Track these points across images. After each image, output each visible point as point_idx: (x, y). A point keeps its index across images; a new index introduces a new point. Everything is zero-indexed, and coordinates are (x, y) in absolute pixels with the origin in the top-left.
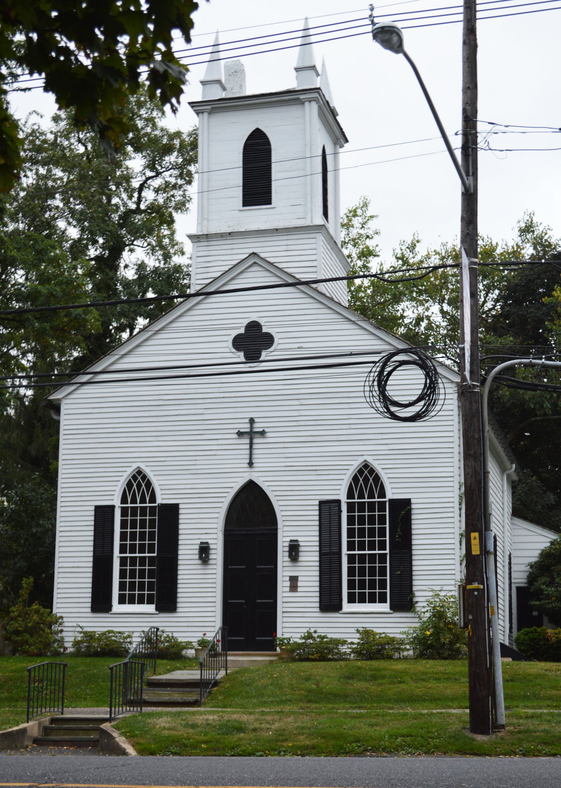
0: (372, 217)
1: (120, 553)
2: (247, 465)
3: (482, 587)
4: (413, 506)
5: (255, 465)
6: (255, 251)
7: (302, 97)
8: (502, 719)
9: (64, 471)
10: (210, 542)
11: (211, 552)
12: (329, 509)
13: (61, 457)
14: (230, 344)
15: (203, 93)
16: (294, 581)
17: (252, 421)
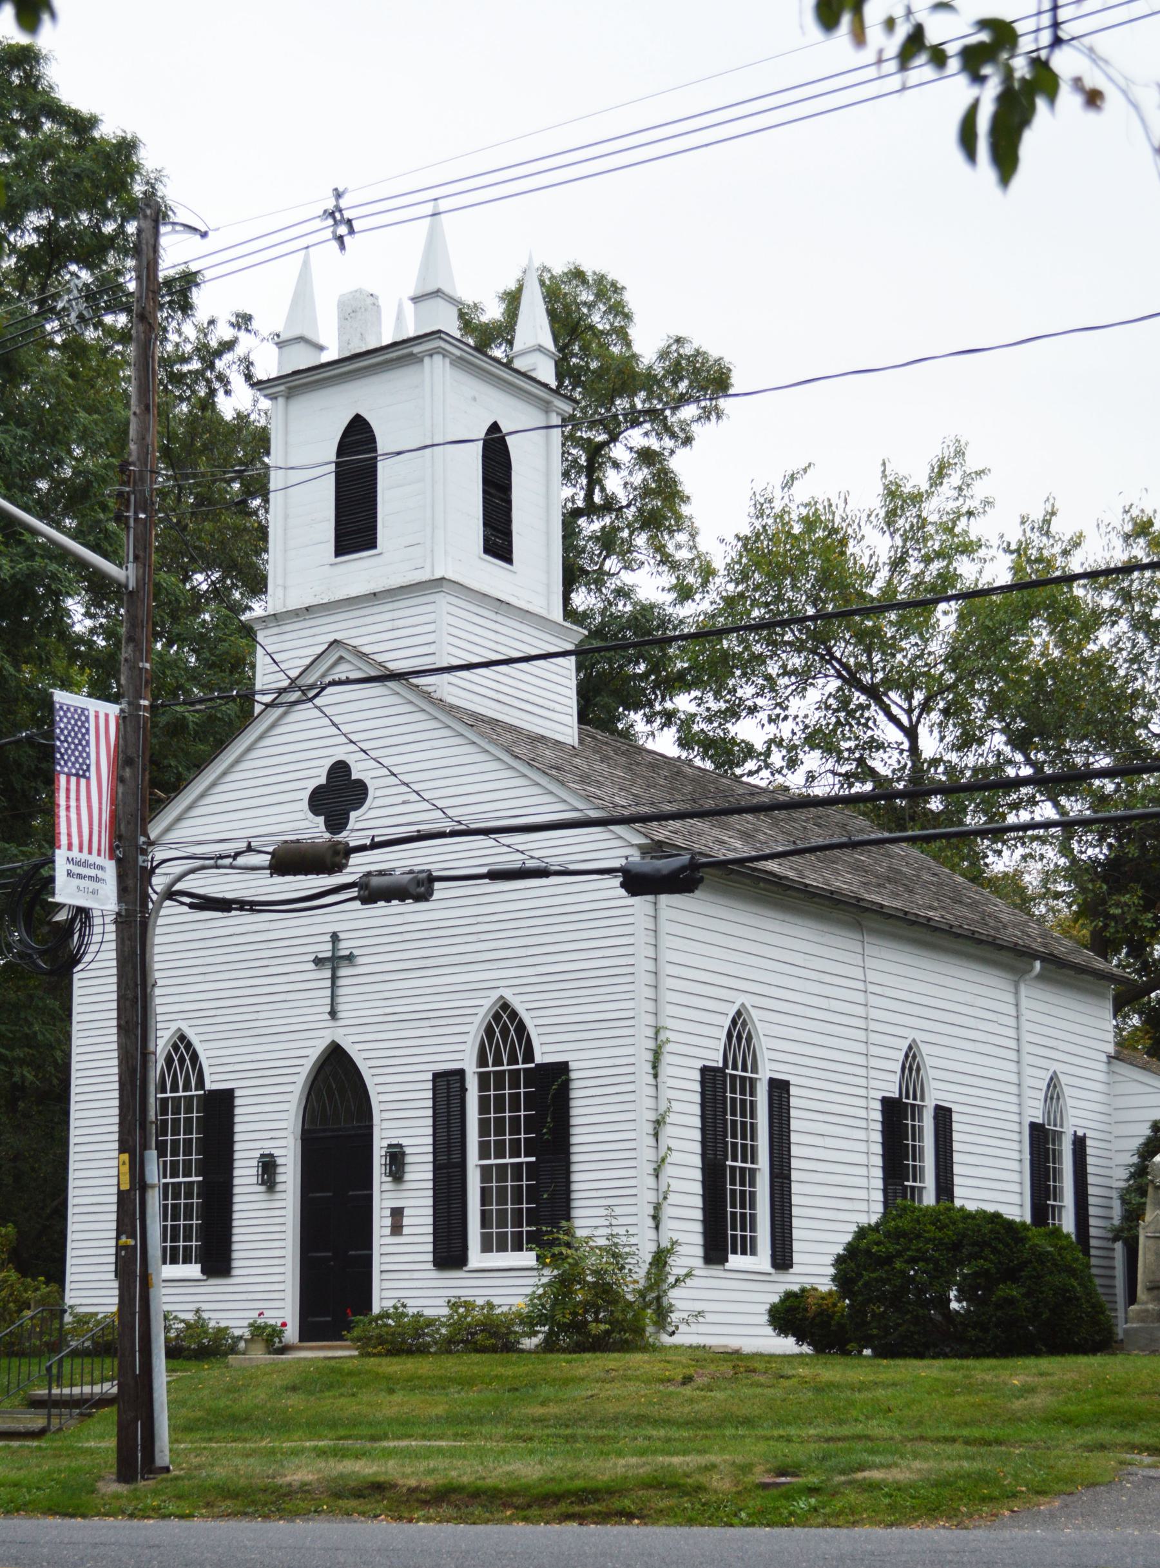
0: (980, 473)
1: (481, 1158)
2: (328, 1017)
3: (131, 1242)
4: (573, 1075)
5: (340, 1015)
6: (338, 636)
7: (416, 350)
8: (163, 1456)
9: (80, 1042)
10: (276, 1152)
11: (280, 1170)
12: (447, 1085)
13: (76, 1018)
14: (305, 805)
15: (279, 363)
16: (397, 1213)
17: (335, 938)
